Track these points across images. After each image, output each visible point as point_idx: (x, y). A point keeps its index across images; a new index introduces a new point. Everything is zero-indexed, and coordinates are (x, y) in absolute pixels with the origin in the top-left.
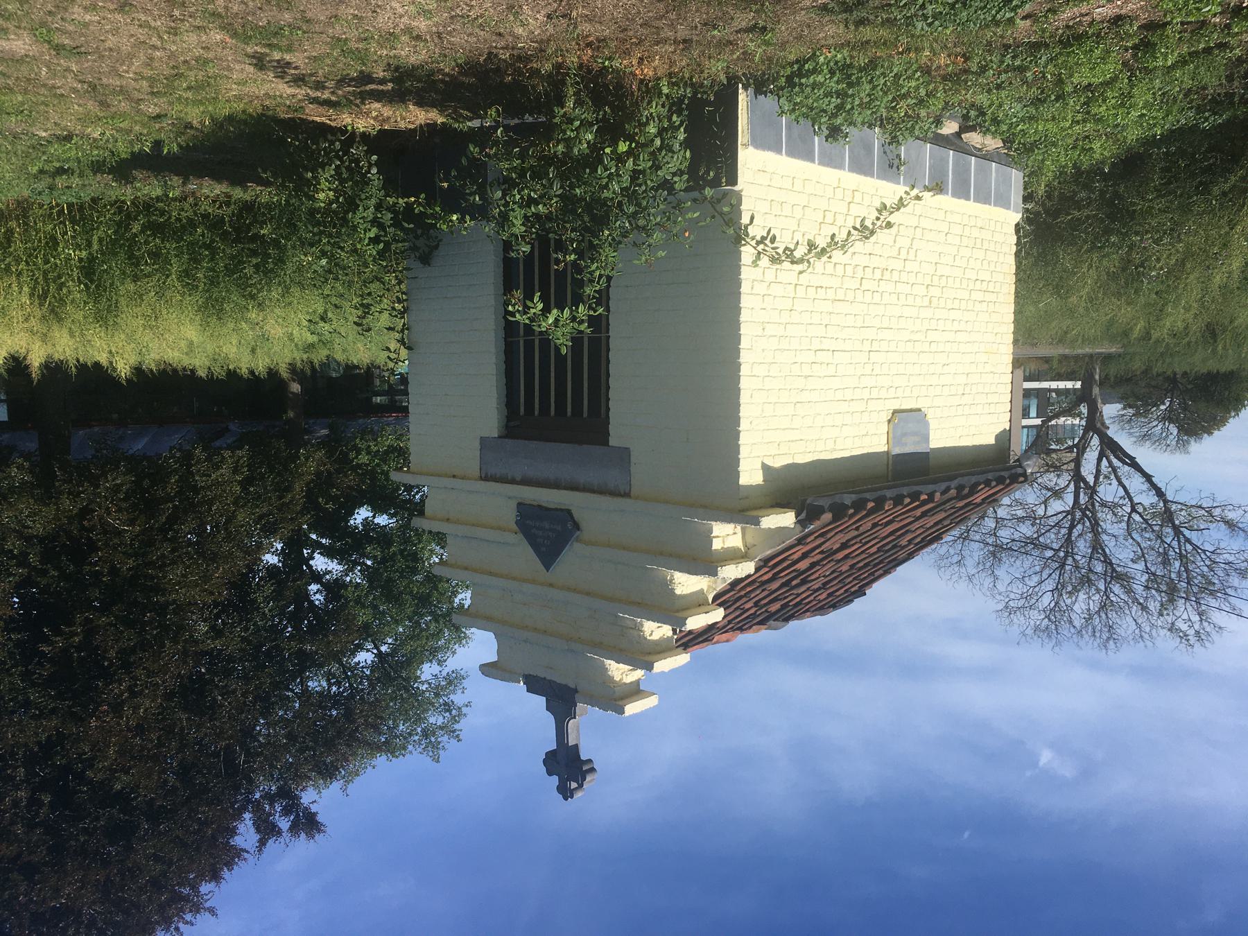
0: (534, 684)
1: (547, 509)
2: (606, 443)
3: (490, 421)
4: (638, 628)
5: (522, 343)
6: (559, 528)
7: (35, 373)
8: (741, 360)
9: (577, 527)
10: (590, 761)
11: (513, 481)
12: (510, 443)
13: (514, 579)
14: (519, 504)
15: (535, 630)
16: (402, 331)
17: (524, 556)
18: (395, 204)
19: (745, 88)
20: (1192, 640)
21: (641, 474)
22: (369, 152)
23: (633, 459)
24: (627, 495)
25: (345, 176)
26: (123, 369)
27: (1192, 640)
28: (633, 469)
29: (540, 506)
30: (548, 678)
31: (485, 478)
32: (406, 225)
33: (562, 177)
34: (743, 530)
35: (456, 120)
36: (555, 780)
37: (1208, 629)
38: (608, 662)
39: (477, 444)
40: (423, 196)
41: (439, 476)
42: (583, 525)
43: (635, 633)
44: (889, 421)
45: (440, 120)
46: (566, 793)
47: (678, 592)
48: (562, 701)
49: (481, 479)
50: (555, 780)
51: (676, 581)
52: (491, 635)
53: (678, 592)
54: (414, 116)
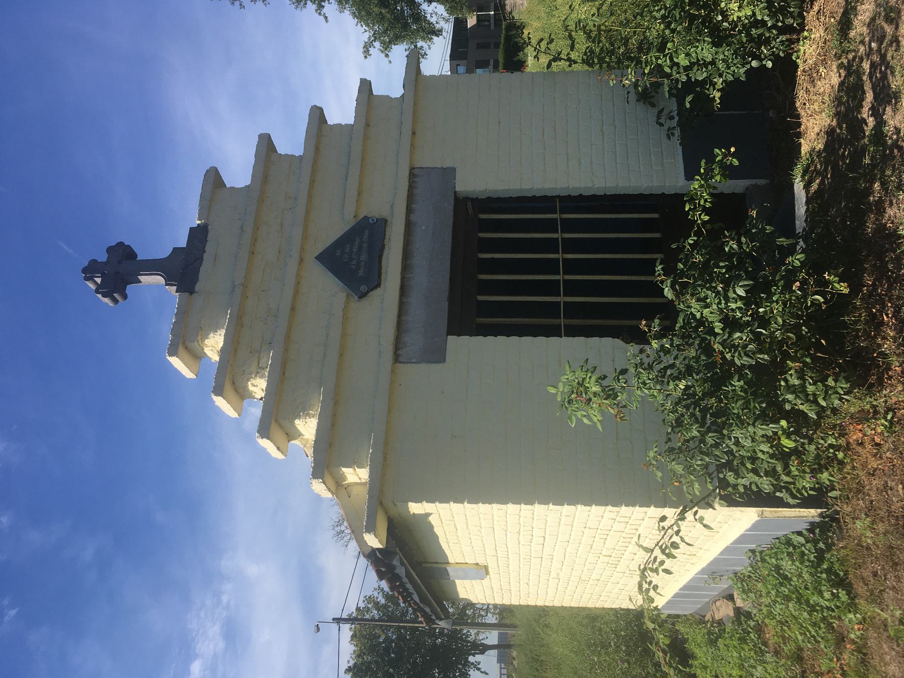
0: (198, 235)
1: (380, 262)
2: (450, 332)
3: (475, 180)
4: (258, 373)
5: (555, 236)
6: (361, 273)
7: (743, 79)
8: (536, 505)
9: (362, 296)
10: (125, 297)
11: (409, 211)
12: (449, 206)
13: (308, 212)
14: (385, 221)
15: (255, 240)
16: (569, 59)
17: (330, 228)
18: (713, 85)
19: (821, 515)
20: (338, 529)
21: (417, 374)
22: (775, 58)
23: (433, 366)
24: (397, 358)
25: (754, 31)
26: (652, 508)
27: (338, 529)
28: (423, 366)
29: (383, 247)
30: (205, 256)
31: (412, 175)
32: (689, 98)
33: (757, 368)
34: (365, 484)
35: (805, 171)
36: (103, 257)
37: (345, 538)
38: (223, 332)
39: (446, 165)
40: (736, 162)
41: (415, 104)
42: (365, 302)
43: (254, 368)
44: (477, 564)
45: (805, 149)
46: (90, 271)
47: (297, 422)
48: (184, 269)
49: (412, 169)
50: (103, 257)
51: (308, 420)
52: (248, 183)
53: (297, 422)
54: (815, 123)
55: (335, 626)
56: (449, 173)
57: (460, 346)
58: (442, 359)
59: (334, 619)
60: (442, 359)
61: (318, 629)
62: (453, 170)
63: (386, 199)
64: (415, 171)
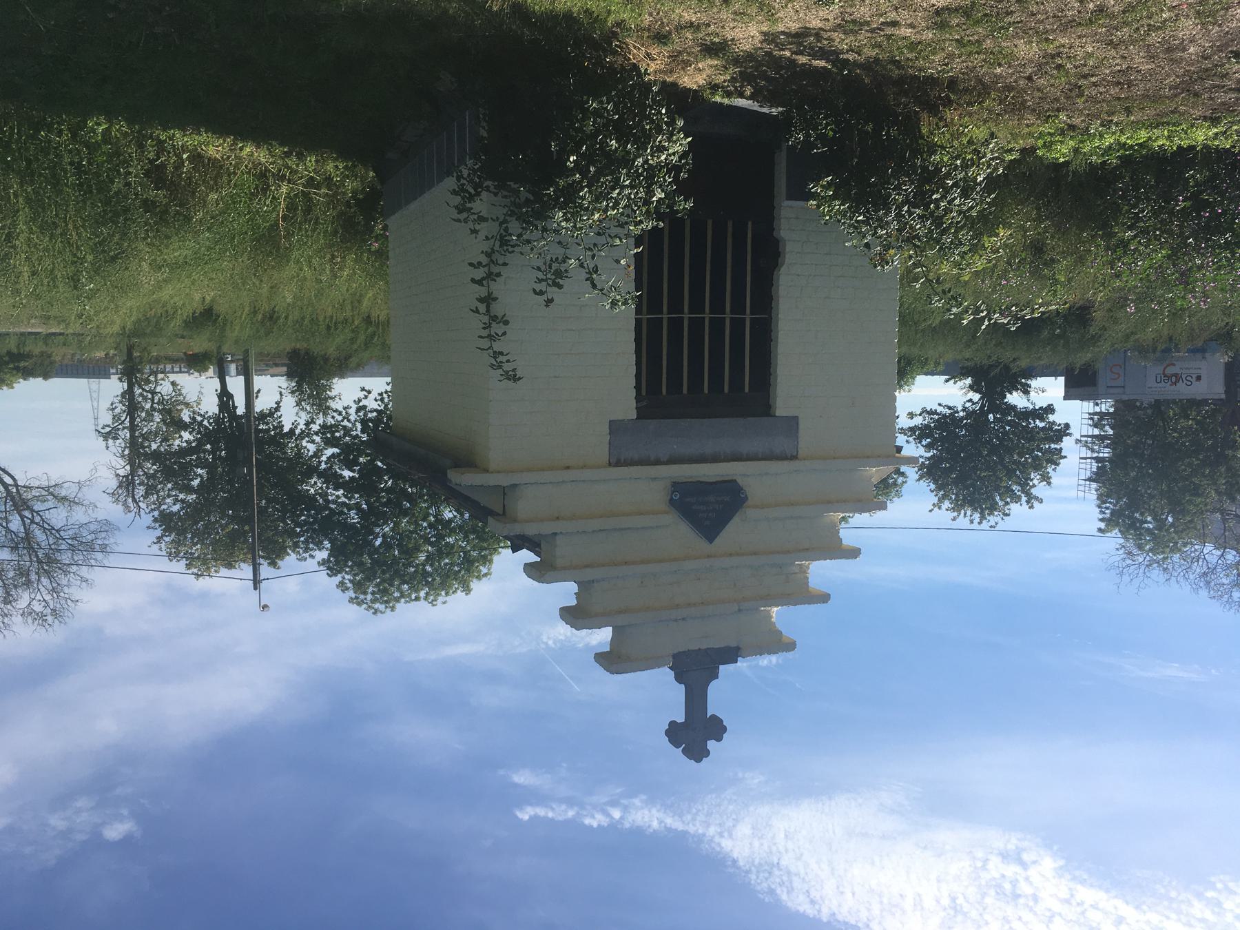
11: (657, 462)
12: (652, 424)
17: (677, 534)
21: (807, 439)
24: (794, 458)
27: (50, 618)
31: (618, 463)
55: (264, 585)
56: (616, 427)
57: (783, 405)
58: (795, 419)
59: (255, 588)
60: (795, 419)
61: (265, 607)
62: (612, 423)
63: (646, 487)
64: (613, 461)
